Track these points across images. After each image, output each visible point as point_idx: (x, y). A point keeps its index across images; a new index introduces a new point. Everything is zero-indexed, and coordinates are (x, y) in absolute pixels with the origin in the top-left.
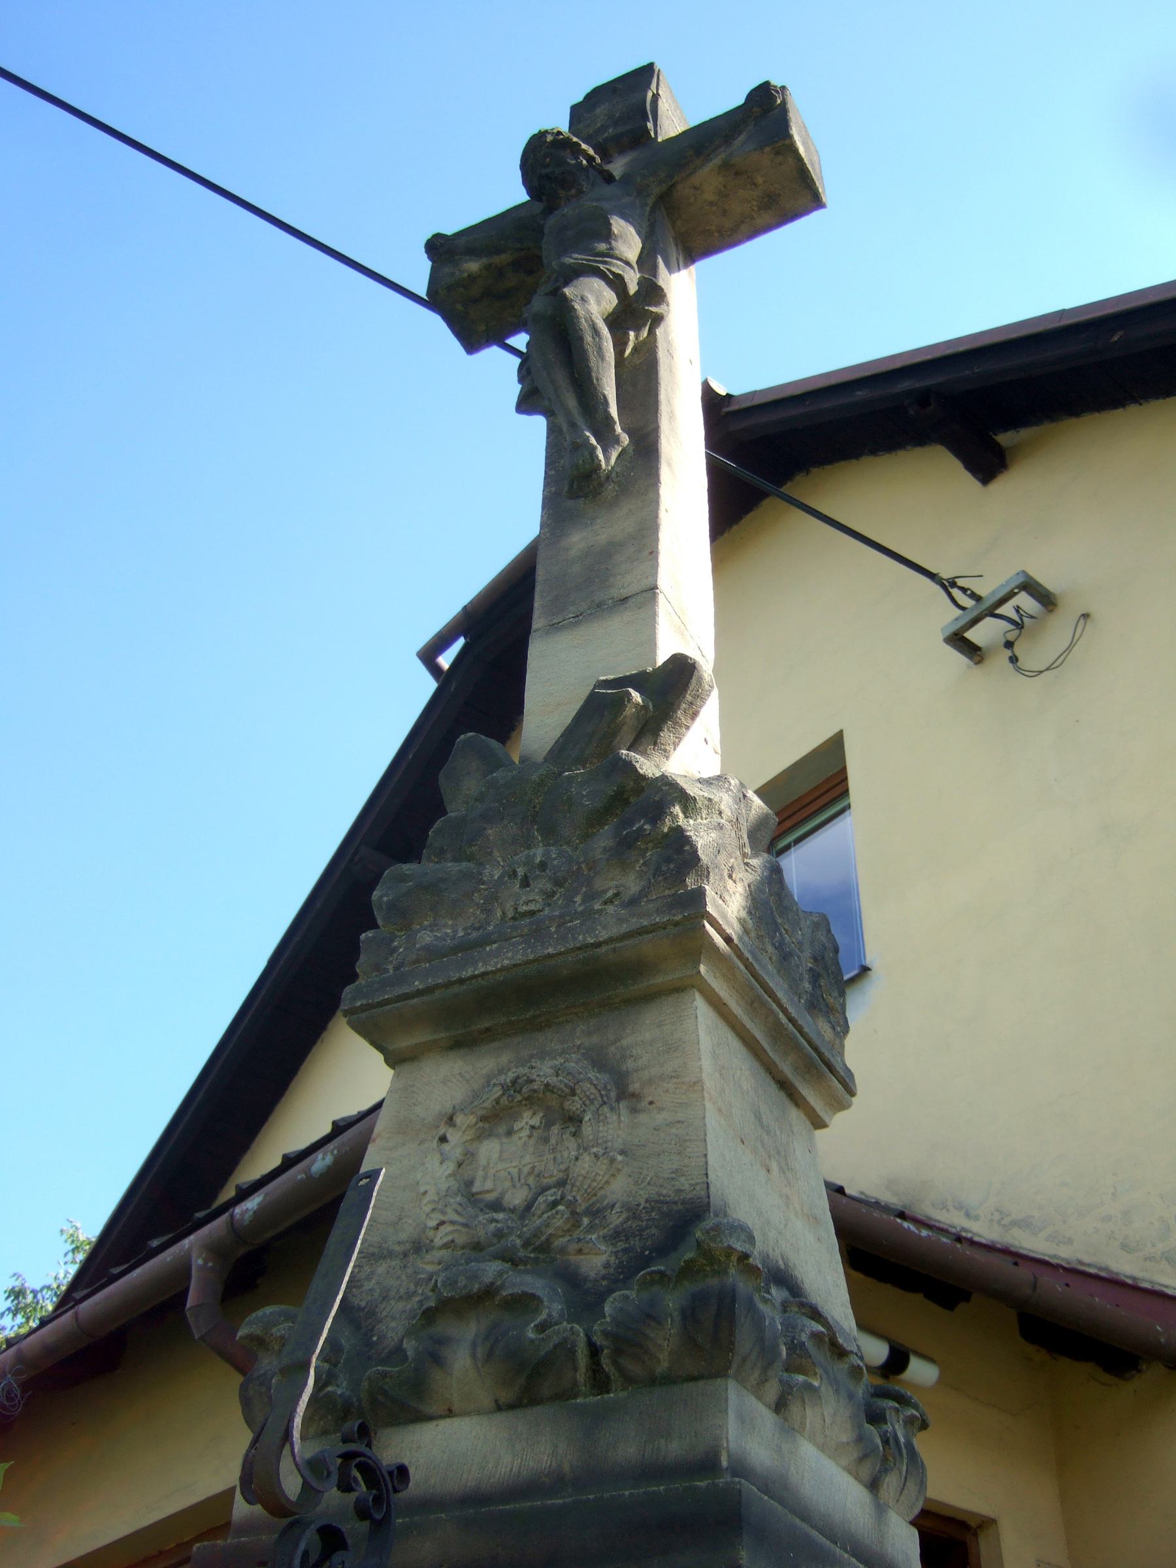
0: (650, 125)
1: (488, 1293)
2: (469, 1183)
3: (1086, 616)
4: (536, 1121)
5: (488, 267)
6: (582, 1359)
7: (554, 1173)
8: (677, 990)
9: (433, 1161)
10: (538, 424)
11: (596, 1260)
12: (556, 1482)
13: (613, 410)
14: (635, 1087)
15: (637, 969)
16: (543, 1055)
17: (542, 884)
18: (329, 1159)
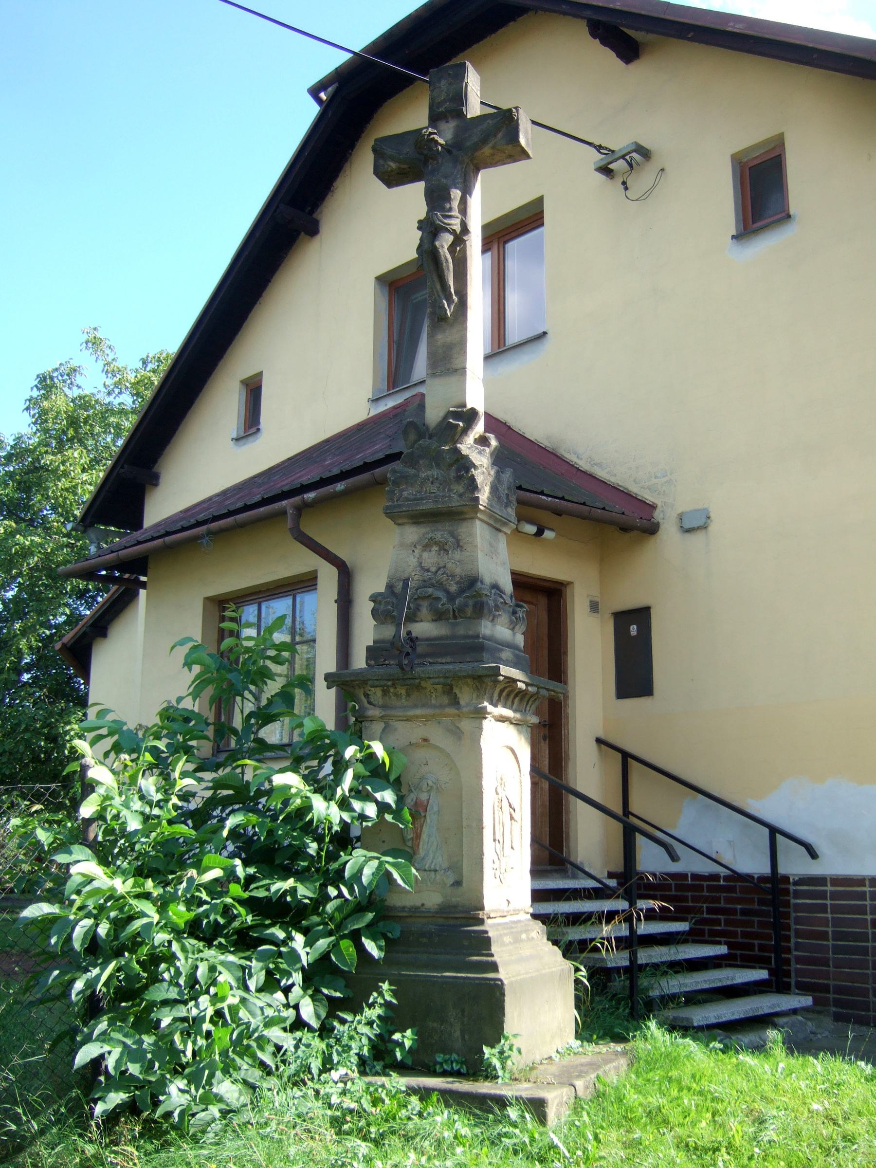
0: (464, 108)
1: (430, 596)
2: (421, 563)
3: (662, 170)
4: (437, 549)
5: (399, 168)
6: (451, 613)
7: (442, 564)
8: (472, 518)
9: (412, 558)
10: (420, 233)
11: (453, 588)
12: (446, 638)
13: (452, 290)
14: (461, 544)
15: (462, 513)
16: (438, 530)
17: (437, 485)
18: (343, 487)
